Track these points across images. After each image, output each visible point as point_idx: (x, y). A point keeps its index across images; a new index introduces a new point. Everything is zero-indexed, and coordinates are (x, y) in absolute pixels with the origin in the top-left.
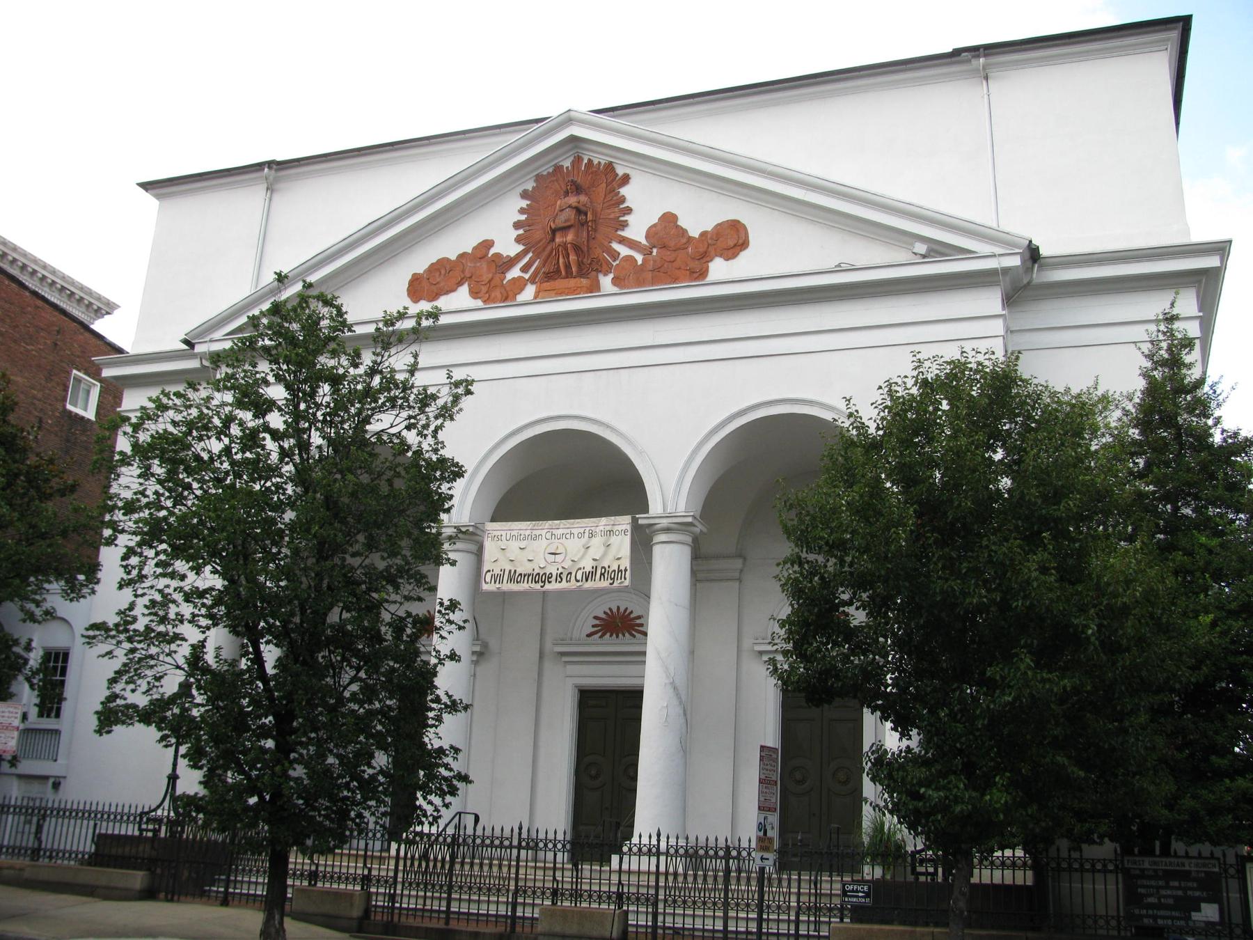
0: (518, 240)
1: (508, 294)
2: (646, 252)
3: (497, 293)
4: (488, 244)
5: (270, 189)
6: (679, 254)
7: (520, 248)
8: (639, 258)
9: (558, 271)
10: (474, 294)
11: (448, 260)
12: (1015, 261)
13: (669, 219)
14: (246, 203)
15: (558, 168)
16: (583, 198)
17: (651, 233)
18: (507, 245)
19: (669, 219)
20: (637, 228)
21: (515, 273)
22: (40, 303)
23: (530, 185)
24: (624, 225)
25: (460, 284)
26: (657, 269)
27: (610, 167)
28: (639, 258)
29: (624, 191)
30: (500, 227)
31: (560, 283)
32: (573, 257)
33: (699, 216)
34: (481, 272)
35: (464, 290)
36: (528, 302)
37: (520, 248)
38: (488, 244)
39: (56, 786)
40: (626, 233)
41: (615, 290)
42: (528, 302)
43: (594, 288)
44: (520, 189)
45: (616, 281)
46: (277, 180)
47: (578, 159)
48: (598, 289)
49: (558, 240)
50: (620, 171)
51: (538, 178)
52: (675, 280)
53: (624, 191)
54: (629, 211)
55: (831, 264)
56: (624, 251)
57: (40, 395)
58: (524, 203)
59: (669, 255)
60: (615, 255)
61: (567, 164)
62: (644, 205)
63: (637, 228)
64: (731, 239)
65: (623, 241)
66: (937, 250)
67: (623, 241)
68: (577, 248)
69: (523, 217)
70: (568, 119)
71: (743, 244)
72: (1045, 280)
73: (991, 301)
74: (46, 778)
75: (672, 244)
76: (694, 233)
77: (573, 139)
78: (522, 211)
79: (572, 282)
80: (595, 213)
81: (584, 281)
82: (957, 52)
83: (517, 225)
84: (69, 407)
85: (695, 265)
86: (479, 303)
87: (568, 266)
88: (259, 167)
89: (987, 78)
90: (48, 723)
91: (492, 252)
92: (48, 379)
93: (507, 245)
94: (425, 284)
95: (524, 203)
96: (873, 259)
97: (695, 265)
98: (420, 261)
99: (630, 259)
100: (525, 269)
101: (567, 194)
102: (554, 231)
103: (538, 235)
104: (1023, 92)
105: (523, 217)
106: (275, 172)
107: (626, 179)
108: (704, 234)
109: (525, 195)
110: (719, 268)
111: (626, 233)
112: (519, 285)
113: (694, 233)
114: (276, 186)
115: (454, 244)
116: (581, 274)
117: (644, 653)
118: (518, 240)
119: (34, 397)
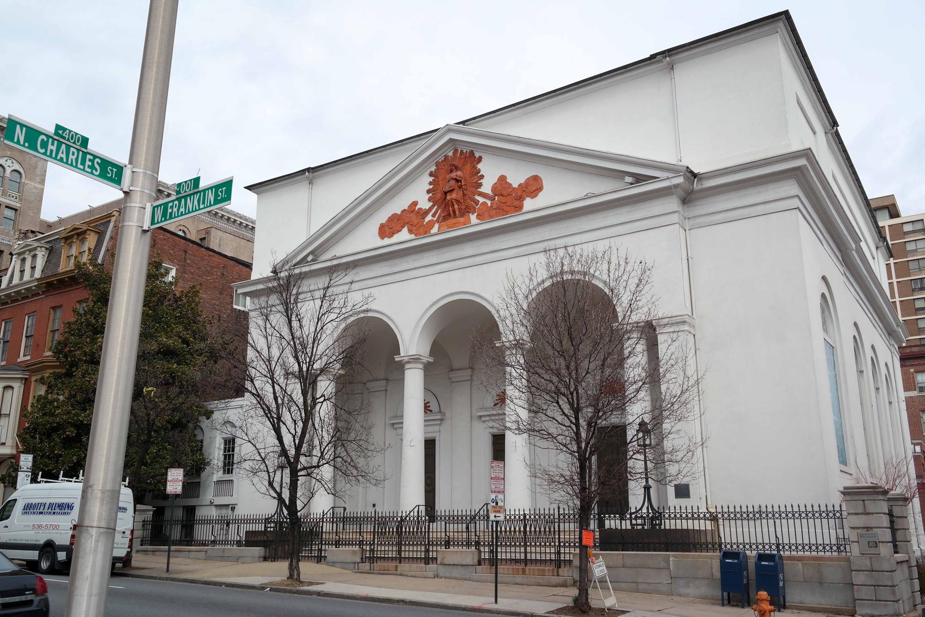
0: (429, 200)
1: (425, 230)
2: (492, 199)
3: (421, 230)
4: (415, 203)
5: (311, 183)
6: (509, 198)
7: (431, 204)
8: (489, 203)
9: (449, 215)
10: (410, 231)
11: (396, 214)
12: (680, 180)
13: (502, 179)
14: (298, 194)
15: (446, 157)
16: (459, 173)
17: (494, 188)
18: (424, 204)
19: (502, 179)
20: (487, 187)
21: (429, 218)
22: (211, 253)
23: (433, 169)
24: (480, 185)
25: (403, 227)
26: (498, 208)
27: (472, 153)
28: (489, 203)
29: (479, 166)
30: (419, 193)
31: (451, 221)
32: (456, 207)
33: (516, 178)
34: (411, 218)
35: (405, 230)
36: (436, 234)
37: (431, 204)
38: (415, 203)
39: (233, 509)
40: (482, 190)
41: (479, 221)
42: (436, 234)
43: (467, 223)
44: (428, 172)
45: (478, 217)
46: (314, 178)
47: (456, 151)
48: (469, 221)
49: (448, 197)
50: (477, 155)
51: (437, 164)
52: (507, 213)
53: (479, 166)
54: (482, 176)
55: (582, 195)
56: (481, 200)
57: (217, 303)
58: (431, 179)
59: (503, 199)
60: (477, 202)
61: (451, 154)
62: (490, 173)
63: (487, 187)
64: (533, 187)
65: (481, 194)
66: (639, 179)
67: (481, 194)
68: (458, 201)
69: (431, 187)
70: (449, 129)
71: (540, 189)
72: (704, 186)
73: (672, 204)
74: (228, 505)
75: (504, 193)
76: (515, 185)
77: (451, 140)
78: (430, 183)
79: (454, 221)
80: (466, 180)
81: (462, 220)
82: (653, 57)
83: (428, 192)
84: (235, 307)
85: (517, 203)
86: (413, 236)
87: (454, 211)
88: (303, 171)
89: (672, 69)
90: (227, 477)
91: (417, 207)
92: (221, 293)
93: (424, 204)
94: (387, 229)
95: (431, 179)
96: (605, 189)
97: (517, 203)
98: (383, 216)
99: (484, 204)
100: (433, 216)
101: (451, 171)
102: (446, 193)
103: (439, 195)
104: (690, 76)
105: (431, 187)
106: (311, 174)
107: (480, 159)
108: (520, 185)
109: (431, 175)
110: (529, 204)
111: (482, 190)
112: (431, 224)
113: (515, 185)
114: (314, 181)
115: (398, 205)
116: (462, 215)
117: (425, 421)
118: (429, 200)
119: (215, 304)
